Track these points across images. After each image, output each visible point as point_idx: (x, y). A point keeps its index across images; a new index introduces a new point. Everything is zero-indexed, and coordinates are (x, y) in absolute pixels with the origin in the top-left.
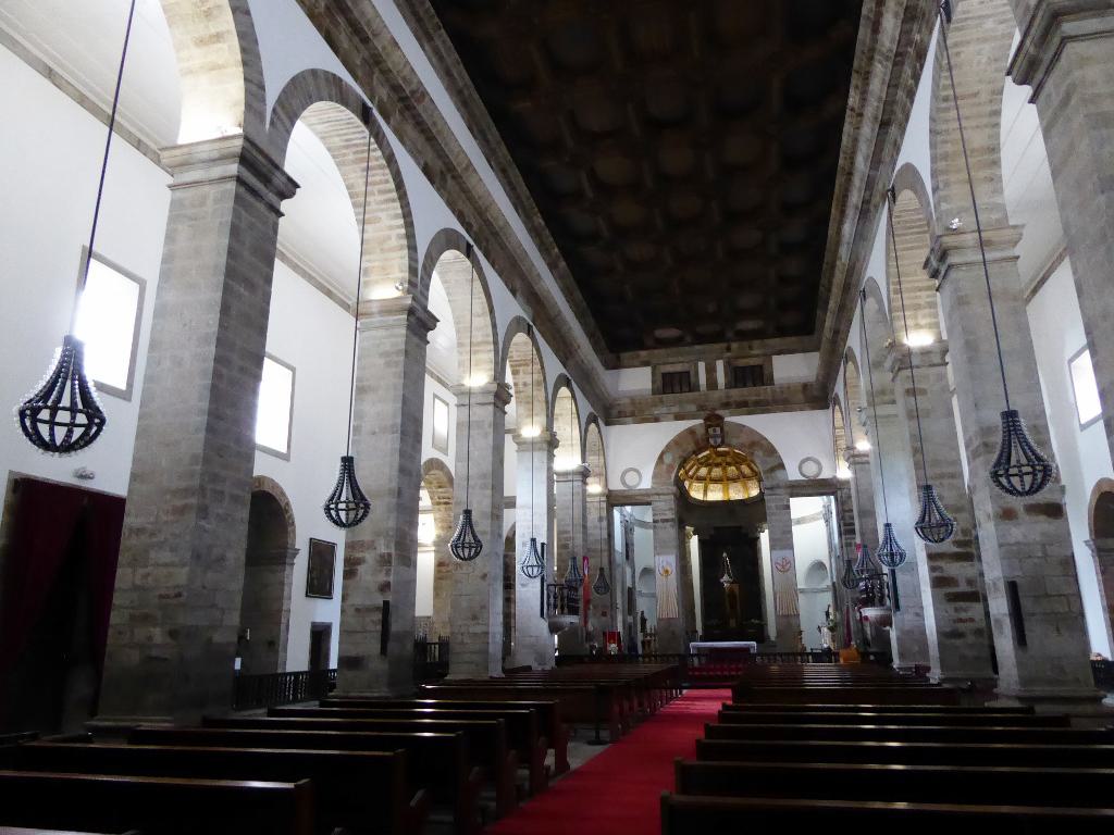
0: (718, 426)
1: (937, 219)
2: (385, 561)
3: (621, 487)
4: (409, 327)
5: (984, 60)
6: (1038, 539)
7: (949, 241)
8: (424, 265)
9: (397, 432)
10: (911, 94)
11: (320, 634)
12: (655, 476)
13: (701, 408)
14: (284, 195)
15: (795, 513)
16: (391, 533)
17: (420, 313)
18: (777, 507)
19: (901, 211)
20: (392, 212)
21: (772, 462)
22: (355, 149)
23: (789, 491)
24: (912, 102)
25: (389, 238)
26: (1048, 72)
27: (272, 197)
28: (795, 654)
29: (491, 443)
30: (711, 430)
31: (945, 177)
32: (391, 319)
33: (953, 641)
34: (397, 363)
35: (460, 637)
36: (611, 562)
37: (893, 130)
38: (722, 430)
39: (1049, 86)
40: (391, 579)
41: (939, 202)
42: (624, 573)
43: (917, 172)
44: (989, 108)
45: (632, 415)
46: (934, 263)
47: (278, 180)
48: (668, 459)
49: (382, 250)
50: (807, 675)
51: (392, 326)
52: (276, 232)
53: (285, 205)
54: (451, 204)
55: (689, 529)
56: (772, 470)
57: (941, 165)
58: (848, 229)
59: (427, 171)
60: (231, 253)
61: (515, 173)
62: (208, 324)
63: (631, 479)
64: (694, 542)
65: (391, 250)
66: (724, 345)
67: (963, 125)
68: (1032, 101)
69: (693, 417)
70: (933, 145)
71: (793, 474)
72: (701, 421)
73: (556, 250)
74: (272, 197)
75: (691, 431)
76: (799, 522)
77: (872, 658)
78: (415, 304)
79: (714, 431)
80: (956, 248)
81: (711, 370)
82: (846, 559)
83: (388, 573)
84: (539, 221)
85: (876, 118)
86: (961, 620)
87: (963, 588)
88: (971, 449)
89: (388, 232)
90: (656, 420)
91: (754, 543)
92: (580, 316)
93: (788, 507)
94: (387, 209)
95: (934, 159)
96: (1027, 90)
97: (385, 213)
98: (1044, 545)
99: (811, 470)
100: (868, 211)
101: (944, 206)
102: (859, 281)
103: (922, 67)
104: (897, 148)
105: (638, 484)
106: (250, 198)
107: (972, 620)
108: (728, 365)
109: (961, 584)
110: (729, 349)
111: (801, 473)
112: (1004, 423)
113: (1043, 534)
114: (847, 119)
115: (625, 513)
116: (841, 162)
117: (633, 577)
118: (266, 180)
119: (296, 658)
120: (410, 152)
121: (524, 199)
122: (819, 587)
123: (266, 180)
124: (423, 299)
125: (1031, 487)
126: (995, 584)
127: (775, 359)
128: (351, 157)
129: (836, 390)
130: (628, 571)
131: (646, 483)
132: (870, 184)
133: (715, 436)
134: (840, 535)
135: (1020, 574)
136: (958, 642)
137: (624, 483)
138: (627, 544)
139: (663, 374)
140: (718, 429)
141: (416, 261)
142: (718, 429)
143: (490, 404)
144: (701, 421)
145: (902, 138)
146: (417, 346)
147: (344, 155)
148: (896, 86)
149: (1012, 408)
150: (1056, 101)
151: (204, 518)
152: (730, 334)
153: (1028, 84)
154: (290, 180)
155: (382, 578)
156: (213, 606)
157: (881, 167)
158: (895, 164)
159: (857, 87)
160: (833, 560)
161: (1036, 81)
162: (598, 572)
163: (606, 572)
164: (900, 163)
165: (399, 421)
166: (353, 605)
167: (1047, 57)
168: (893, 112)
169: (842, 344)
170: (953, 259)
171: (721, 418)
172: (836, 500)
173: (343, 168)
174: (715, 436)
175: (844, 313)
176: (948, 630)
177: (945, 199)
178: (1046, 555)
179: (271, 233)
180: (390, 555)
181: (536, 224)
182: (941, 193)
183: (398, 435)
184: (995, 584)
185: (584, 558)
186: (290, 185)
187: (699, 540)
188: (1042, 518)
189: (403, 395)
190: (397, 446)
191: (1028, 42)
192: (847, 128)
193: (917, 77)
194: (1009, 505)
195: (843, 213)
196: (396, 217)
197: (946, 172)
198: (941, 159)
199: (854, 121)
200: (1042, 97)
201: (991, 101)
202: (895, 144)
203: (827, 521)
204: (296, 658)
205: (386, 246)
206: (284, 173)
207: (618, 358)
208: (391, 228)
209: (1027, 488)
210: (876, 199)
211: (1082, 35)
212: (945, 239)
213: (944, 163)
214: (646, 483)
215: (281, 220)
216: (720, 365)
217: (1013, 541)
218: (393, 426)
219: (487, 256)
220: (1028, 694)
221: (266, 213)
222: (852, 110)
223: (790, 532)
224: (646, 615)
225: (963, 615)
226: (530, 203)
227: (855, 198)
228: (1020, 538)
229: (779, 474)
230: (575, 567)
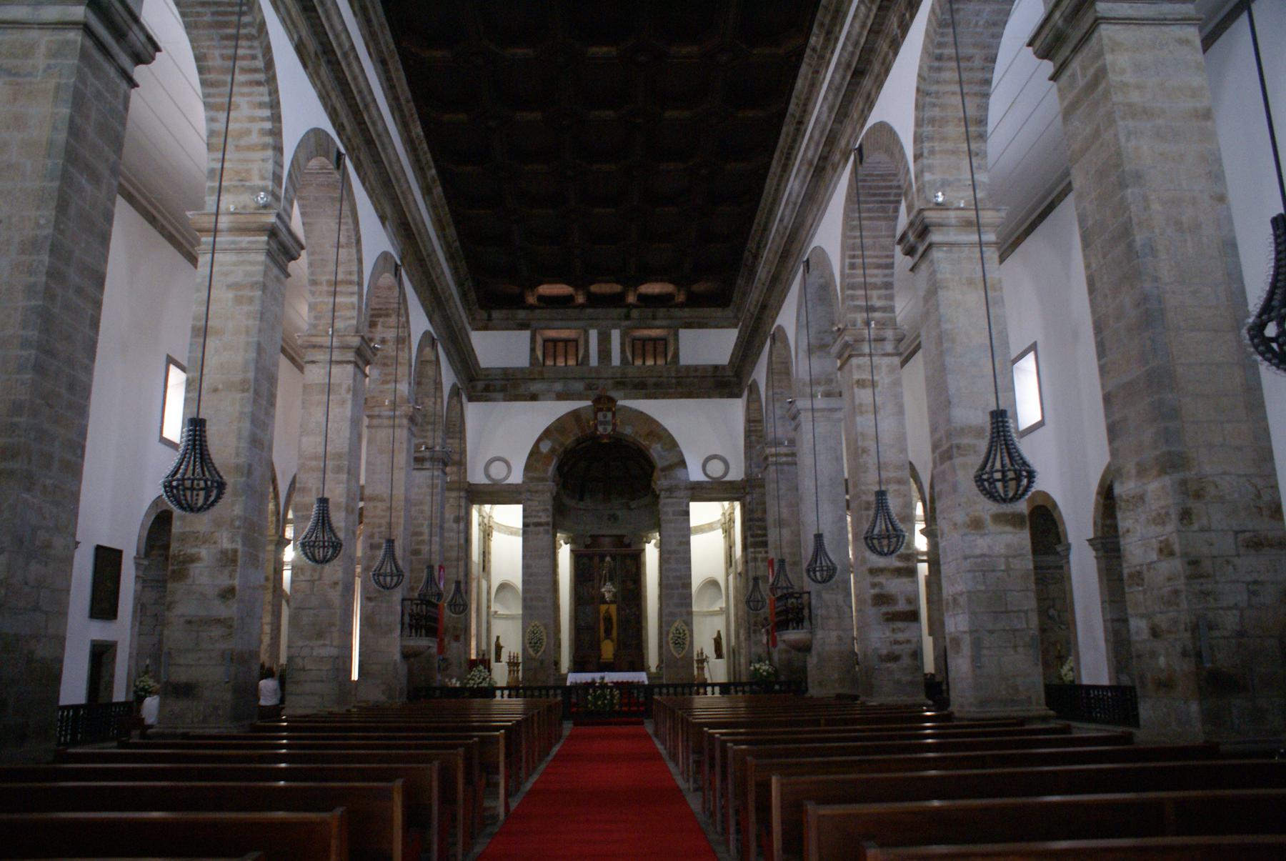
0: (609, 410)
1: (918, 190)
2: (228, 560)
3: (485, 481)
4: (269, 253)
5: (981, 23)
6: (1003, 551)
7: (931, 216)
8: (290, 175)
9: (247, 390)
10: (895, 45)
11: (101, 655)
12: (528, 468)
13: (589, 387)
14: (140, 59)
15: (694, 522)
16: (237, 523)
17: (284, 236)
18: (675, 513)
19: (867, 175)
20: (258, 99)
21: (673, 459)
22: (214, 9)
23: (689, 493)
24: (896, 54)
25: (248, 132)
26: (1076, 50)
27: (125, 61)
28: (691, 686)
29: (348, 413)
30: (600, 415)
31: (931, 144)
32: (245, 240)
33: (889, 665)
34: (251, 300)
35: (299, 661)
36: (467, 573)
37: (867, 83)
38: (614, 414)
39: (1075, 65)
40: (236, 582)
41: (922, 172)
42: (479, 587)
43: (895, 133)
44: (980, 75)
45: (503, 389)
46: (911, 238)
47: (136, 37)
48: (545, 447)
49: (237, 146)
50: (696, 705)
51: (247, 250)
52: (126, 108)
53: (139, 72)
54: (324, 98)
55: (560, 537)
56: (671, 467)
57: (928, 129)
58: (794, 185)
59: (300, 49)
60: (74, 130)
61: (396, 65)
62: (37, 224)
63: (498, 471)
64: (564, 554)
65: (249, 148)
66: (624, 310)
67: (965, 91)
68: (1054, 78)
69: (580, 397)
70: (919, 107)
71: (695, 473)
72: (589, 403)
73: (433, 171)
74: (125, 61)
75: (575, 415)
76: (701, 530)
77: (777, 687)
78: (279, 224)
79: (605, 416)
80: (940, 225)
81: (604, 340)
82: (751, 574)
83: (231, 577)
84: (418, 130)
85: (849, 66)
86: (896, 642)
87: (902, 606)
88: (938, 451)
89: (247, 125)
90: (534, 397)
91: (637, 558)
92: (451, 258)
93: (687, 513)
94: (250, 94)
95: (919, 123)
96: (1048, 67)
97: (246, 99)
98: (1007, 557)
99: (716, 469)
100: (824, 169)
101: (927, 177)
102: (801, 251)
103: (912, 17)
104: (870, 103)
105: (506, 478)
106: (97, 56)
107: (908, 641)
108: (623, 336)
109: (900, 602)
110: (627, 317)
111: (706, 474)
112: (992, 423)
113: (1008, 546)
114: (806, 60)
115: (484, 514)
116: (792, 107)
117: (489, 593)
118: (120, 35)
119: (73, 690)
120: (283, 21)
121: (403, 102)
122: (711, 609)
123: (120, 35)
124: (286, 218)
125: (1016, 494)
126: (955, 600)
127: (684, 334)
128: (208, 18)
129: (755, 375)
130: (484, 584)
131: (517, 477)
132: (831, 139)
133: (605, 423)
134: (745, 547)
135: (983, 588)
136: (893, 666)
137: (488, 476)
138: (484, 552)
139: (546, 341)
140: (609, 415)
141: (282, 166)
142: (609, 415)
143: (349, 362)
144: (589, 403)
145: (878, 93)
146: (277, 278)
147: (198, 14)
148: (878, 33)
149: (1001, 407)
150: (1081, 83)
151: (29, 490)
152: (631, 299)
153: (1051, 59)
154: (150, 39)
155: (224, 581)
156: (36, 608)
157: (847, 121)
158: (865, 120)
159: (822, 25)
160: (731, 577)
161: (1061, 57)
162: (453, 586)
163: (462, 586)
164: (873, 120)
165: (251, 375)
166: (182, 616)
167: (1075, 35)
168: (869, 62)
169: (770, 320)
170: (935, 237)
171: (612, 401)
172: (743, 507)
173: (195, 32)
174: (605, 423)
175: (778, 285)
176: (884, 652)
177: (930, 168)
178: (1008, 569)
179: (121, 107)
180: (235, 551)
181: (414, 135)
182: (926, 162)
183: (250, 394)
184: (955, 600)
185: (441, 567)
186: (150, 48)
187: (572, 551)
188: (1009, 528)
189: (259, 344)
190: (248, 409)
191: (1057, 15)
192: (804, 68)
193: (905, 27)
194: (977, 514)
195: (786, 168)
196: (261, 105)
197: (931, 139)
198: (928, 123)
199: (814, 63)
200: (1065, 77)
201: (983, 69)
202: (869, 96)
203: (728, 532)
204: (73, 690)
205: (243, 142)
206: (142, 28)
207: (490, 318)
208: (252, 119)
209: (1011, 494)
210: (837, 157)
211: (1115, 19)
212: (927, 214)
213: (930, 128)
214: (517, 477)
215: (134, 92)
216: (616, 335)
217: (978, 552)
218: (244, 381)
219: (357, 169)
220: (983, 715)
221: (118, 80)
222: (814, 50)
223: (688, 543)
224: (502, 642)
225: (900, 636)
226: (410, 108)
227: (807, 149)
228: (986, 551)
229: (679, 473)
230: (431, 579)
